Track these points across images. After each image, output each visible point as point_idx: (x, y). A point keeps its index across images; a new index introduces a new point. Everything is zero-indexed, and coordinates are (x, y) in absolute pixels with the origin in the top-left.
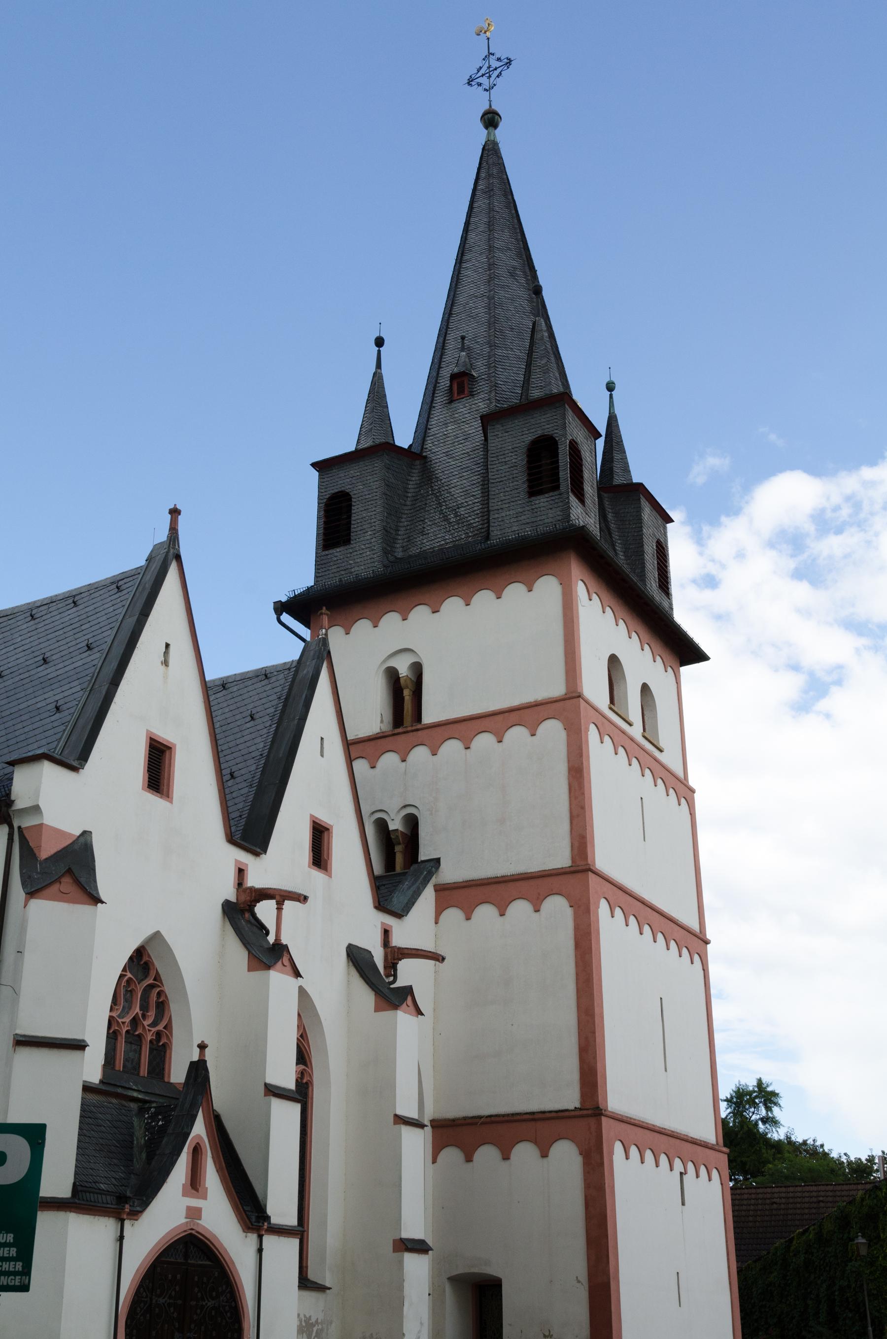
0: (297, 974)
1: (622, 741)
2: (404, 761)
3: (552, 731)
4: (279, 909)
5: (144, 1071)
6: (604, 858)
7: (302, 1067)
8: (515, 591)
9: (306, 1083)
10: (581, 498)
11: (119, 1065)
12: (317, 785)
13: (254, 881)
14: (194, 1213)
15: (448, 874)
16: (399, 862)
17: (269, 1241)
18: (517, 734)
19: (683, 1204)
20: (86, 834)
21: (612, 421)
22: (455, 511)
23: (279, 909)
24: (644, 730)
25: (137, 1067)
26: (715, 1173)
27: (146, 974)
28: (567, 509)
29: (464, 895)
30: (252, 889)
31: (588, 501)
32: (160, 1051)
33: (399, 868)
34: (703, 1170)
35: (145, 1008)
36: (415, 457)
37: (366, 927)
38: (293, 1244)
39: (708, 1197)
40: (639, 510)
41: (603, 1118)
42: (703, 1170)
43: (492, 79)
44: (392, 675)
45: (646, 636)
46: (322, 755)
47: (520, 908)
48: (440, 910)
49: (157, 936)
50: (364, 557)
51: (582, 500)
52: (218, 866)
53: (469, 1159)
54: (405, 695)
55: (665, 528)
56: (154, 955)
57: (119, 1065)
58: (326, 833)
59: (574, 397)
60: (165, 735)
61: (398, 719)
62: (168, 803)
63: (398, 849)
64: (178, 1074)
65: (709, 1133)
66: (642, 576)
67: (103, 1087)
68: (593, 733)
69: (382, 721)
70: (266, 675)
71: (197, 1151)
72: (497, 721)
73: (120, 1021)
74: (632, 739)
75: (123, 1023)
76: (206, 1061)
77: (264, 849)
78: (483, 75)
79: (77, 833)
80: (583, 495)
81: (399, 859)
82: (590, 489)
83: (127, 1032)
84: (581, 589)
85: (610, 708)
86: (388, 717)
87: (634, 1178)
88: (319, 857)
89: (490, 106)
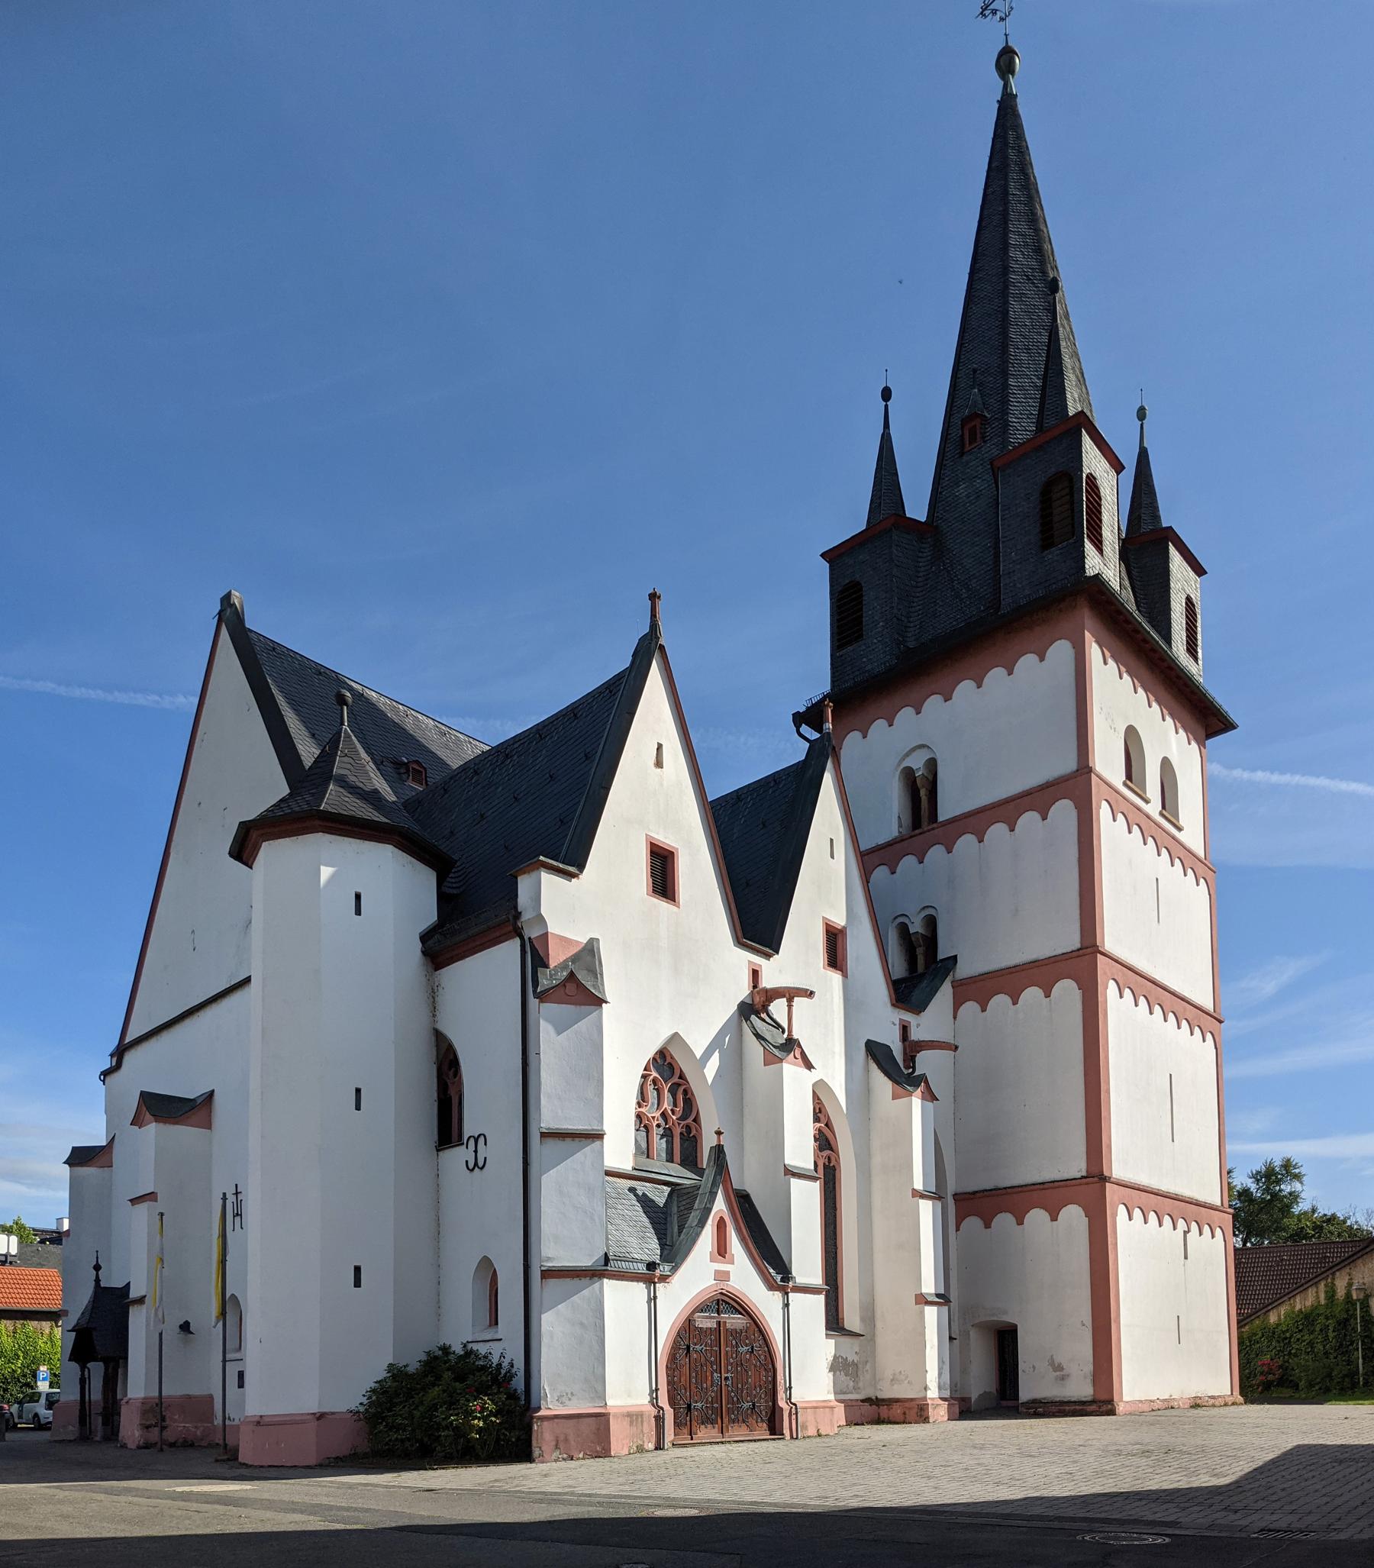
0: (809, 1066)
1: (1137, 821)
2: (921, 862)
4: (790, 1006)
6: (1113, 938)
7: (827, 1152)
12: (825, 881)
13: (767, 982)
14: (722, 1276)
15: (963, 970)
16: (919, 966)
17: (793, 1297)
18: (1029, 819)
19: (1186, 1258)
23: (790, 1006)
24: (1164, 807)
26: (1218, 1232)
28: (1081, 557)
29: (979, 989)
30: (766, 991)
33: (921, 968)
34: (1206, 1229)
38: (820, 1300)
39: (1213, 1251)
42: (1206, 1229)
44: (909, 775)
46: (832, 857)
48: (957, 1005)
49: (675, 1037)
51: (1100, 549)
54: (921, 791)
61: (916, 823)
63: (920, 951)
65: (1212, 1194)
66: (1168, 639)
69: (900, 826)
71: (721, 1225)
72: (1007, 810)
74: (1148, 817)
79: (583, 940)
80: (1101, 542)
84: (1094, 652)
86: (907, 820)
87: (1133, 1236)
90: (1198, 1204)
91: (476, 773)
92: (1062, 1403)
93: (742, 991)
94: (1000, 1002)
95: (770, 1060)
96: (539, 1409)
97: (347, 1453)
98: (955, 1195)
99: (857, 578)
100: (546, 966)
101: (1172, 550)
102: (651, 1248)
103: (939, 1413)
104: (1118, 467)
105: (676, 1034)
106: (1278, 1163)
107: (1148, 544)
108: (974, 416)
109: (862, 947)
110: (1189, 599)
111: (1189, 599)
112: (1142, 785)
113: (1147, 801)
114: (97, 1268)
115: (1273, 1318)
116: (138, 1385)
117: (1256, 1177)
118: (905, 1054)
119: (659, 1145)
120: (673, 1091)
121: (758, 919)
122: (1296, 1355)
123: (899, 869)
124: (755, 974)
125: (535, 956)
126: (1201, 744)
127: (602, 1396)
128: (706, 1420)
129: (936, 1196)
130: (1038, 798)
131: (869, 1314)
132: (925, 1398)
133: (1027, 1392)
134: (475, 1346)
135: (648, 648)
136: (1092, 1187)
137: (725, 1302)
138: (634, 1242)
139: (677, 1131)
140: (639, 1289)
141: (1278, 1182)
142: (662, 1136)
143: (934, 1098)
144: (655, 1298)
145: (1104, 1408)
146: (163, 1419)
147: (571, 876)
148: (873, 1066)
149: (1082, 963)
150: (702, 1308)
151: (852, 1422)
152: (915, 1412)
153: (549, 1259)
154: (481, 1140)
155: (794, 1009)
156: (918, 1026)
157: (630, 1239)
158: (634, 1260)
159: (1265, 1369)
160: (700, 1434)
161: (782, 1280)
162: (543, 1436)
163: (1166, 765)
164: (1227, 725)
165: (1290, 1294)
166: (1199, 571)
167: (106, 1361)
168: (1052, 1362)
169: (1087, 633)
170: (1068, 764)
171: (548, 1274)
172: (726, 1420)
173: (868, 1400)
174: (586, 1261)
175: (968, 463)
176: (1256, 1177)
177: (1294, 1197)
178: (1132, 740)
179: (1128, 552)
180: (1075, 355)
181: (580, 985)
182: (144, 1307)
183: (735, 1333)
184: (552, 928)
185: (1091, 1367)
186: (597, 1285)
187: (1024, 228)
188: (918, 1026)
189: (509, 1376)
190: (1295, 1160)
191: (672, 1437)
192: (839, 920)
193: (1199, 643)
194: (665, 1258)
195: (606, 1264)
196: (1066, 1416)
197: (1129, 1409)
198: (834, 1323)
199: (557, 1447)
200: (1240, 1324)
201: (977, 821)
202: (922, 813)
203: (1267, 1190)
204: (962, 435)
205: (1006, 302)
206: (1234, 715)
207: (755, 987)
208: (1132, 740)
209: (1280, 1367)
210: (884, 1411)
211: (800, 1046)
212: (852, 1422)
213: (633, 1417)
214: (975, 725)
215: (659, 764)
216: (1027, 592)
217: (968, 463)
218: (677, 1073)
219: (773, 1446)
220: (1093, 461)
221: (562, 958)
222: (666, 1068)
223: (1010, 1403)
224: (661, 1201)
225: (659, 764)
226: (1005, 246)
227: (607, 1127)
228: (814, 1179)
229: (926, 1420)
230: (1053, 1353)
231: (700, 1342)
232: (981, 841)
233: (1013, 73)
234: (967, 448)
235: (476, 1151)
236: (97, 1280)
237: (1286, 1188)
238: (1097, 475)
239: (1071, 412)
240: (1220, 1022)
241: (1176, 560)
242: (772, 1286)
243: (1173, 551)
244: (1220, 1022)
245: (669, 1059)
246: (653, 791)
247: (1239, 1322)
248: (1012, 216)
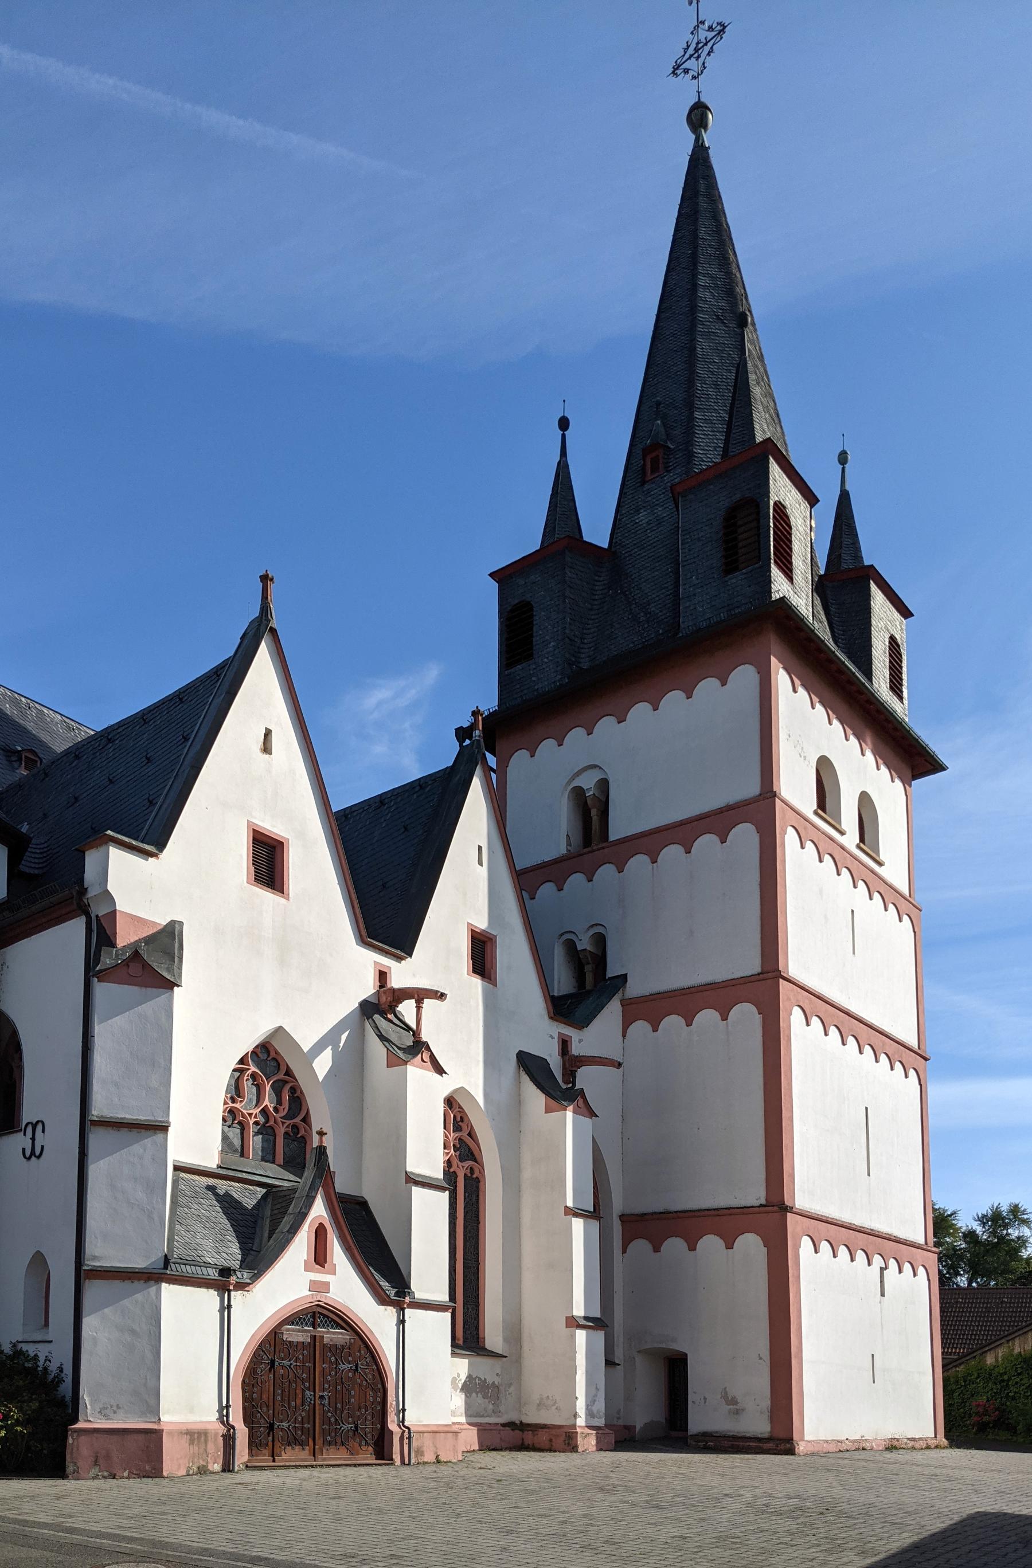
0: (440, 1070)
1: (828, 850)
2: (590, 880)
4: (419, 1008)
10: (788, 571)
12: (466, 888)
13: (396, 982)
15: (635, 988)
16: (583, 982)
18: (707, 842)
19: (883, 1295)
21: (844, 499)
23: (419, 1008)
26: (921, 1271)
28: (767, 582)
29: (651, 1009)
30: (394, 991)
33: (589, 985)
36: (607, 560)
40: (867, 596)
41: (789, 1214)
42: (907, 1267)
43: (695, 41)
44: (578, 793)
50: (546, 672)
51: (790, 578)
54: (591, 810)
58: (489, 944)
61: (587, 839)
62: (282, 901)
63: (588, 969)
65: (915, 1228)
66: (869, 674)
67: (221, 1171)
69: (569, 844)
70: (420, 786)
71: (320, 1233)
73: (245, 1112)
74: (843, 848)
75: (250, 1115)
76: (325, 1148)
77: (161, 844)
78: (689, 58)
79: (163, 922)
80: (791, 571)
81: (589, 978)
85: (858, 847)
86: (577, 839)
90: (897, 1241)
91: (77, 757)
92: (735, 1438)
93: (368, 988)
94: (673, 1022)
95: (393, 1061)
96: (76, 1420)
98: (622, 1217)
99: (524, 600)
100: (113, 945)
101: (873, 587)
102: (232, 1252)
103: (588, 1442)
104: (812, 499)
105: (280, 1029)
106: (1005, 1208)
107: (847, 581)
108: (655, 446)
109: (514, 954)
110: (892, 639)
111: (892, 639)
112: (838, 817)
113: (842, 833)
115: (990, 1360)
117: (983, 1220)
119: (255, 1142)
120: (277, 1090)
121: (389, 912)
122: (1013, 1398)
123: (566, 887)
124: (383, 976)
125: (101, 933)
126: (906, 782)
127: (154, 1409)
128: (293, 1441)
129: (595, 1214)
130: (719, 821)
131: (514, 1333)
132: (574, 1426)
133: (698, 1422)
134: (25, 1347)
135: (260, 628)
136: (771, 1217)
137: (320, 1315)
138: (208, 1244)
139: (281, 1131)
140: (210, 1298)
141: (1006, 1226)
142: (256, 1134)
143: (592, 1114)
144: (229, 1306)
145: (782, 1447)
147: (149, 854)
148: (525, 1079)
149: (763, 986)
150: (294, 1319)
151: (485, 1446)
152: (563, 1440)
153: (95, 1258)
154: (39, 1127)
155: (424, 1011)
156: (580, 1041)
157: (203, 1242)
158: (208, 1265)
159: (981, 1410)
160: (284, 1457)
161: (397, 1294)
162: (79, 1450)
163: (865, 801)
164: (934, 766)
165: (1009, 1336)
166: (905, 612)
168: (725, 1396)
169: (773, 658)
170: (752, 788)
172: (319, 1441)
173: (511, 1425)
174: (139, 1263)
175: (649, 491)
176: (983, 1220)
177: (1022, 1241)
179: (821, 586)
180: (769, 395)
181: (146, 966)
183: (333, 1349)
184: (122, 905)
185: (769, 1403)
186: (153, 1290)
187: (714, 271)
188: (580, 1041)
189: (58, 1380)
190: (1024, 1205)
191: (246, 1458)
192: (482, 924)
193: (905, 683)
194: (244, 1264)
195: (166, 1267)
196: (736, 1452)
197: (811, 1449)
198: (468, 1338)
199: (96, 1463)
200: (945, 1367)
201: (651, 842)
202: (593, 830)
203: (994, 1233)
204: (644, 465)
205: (693, 340)
207: (381, 987)
209: (997, 1409)
210: (529, 1438)
211: (428, 1048)
212: (485, 1446)
213: (195, 1436)
214: (649, 748)
215: (267, 749)
216: (708, 615)
217: (649, 491)
218: (283, 1070)
219: (376, 1474)
220: (781, 488)
221: (133, 939)
222: (269, 1063)
224: (249, 1202)
225: (267, 749)
226: (694, 287)
227: (172, 1119)
228: (441, 1189)
229: (574, 1449)
230: (726, 1383)
231: (288, 1356)
232: (654, 861)
233: (705, 127)
234: (649, 477)
235: (33, 1139)
237: (1014, 1233)
238: (787, 503)
239: (759, 438)
240: (926, 1059)
241: (878, 600)
242: (383, 1300)
243: (874, 588)
244: (926, 1059)
245: (273, 1054)
246: (256, 772)
247: (944, 1366)
248: (701, 259)
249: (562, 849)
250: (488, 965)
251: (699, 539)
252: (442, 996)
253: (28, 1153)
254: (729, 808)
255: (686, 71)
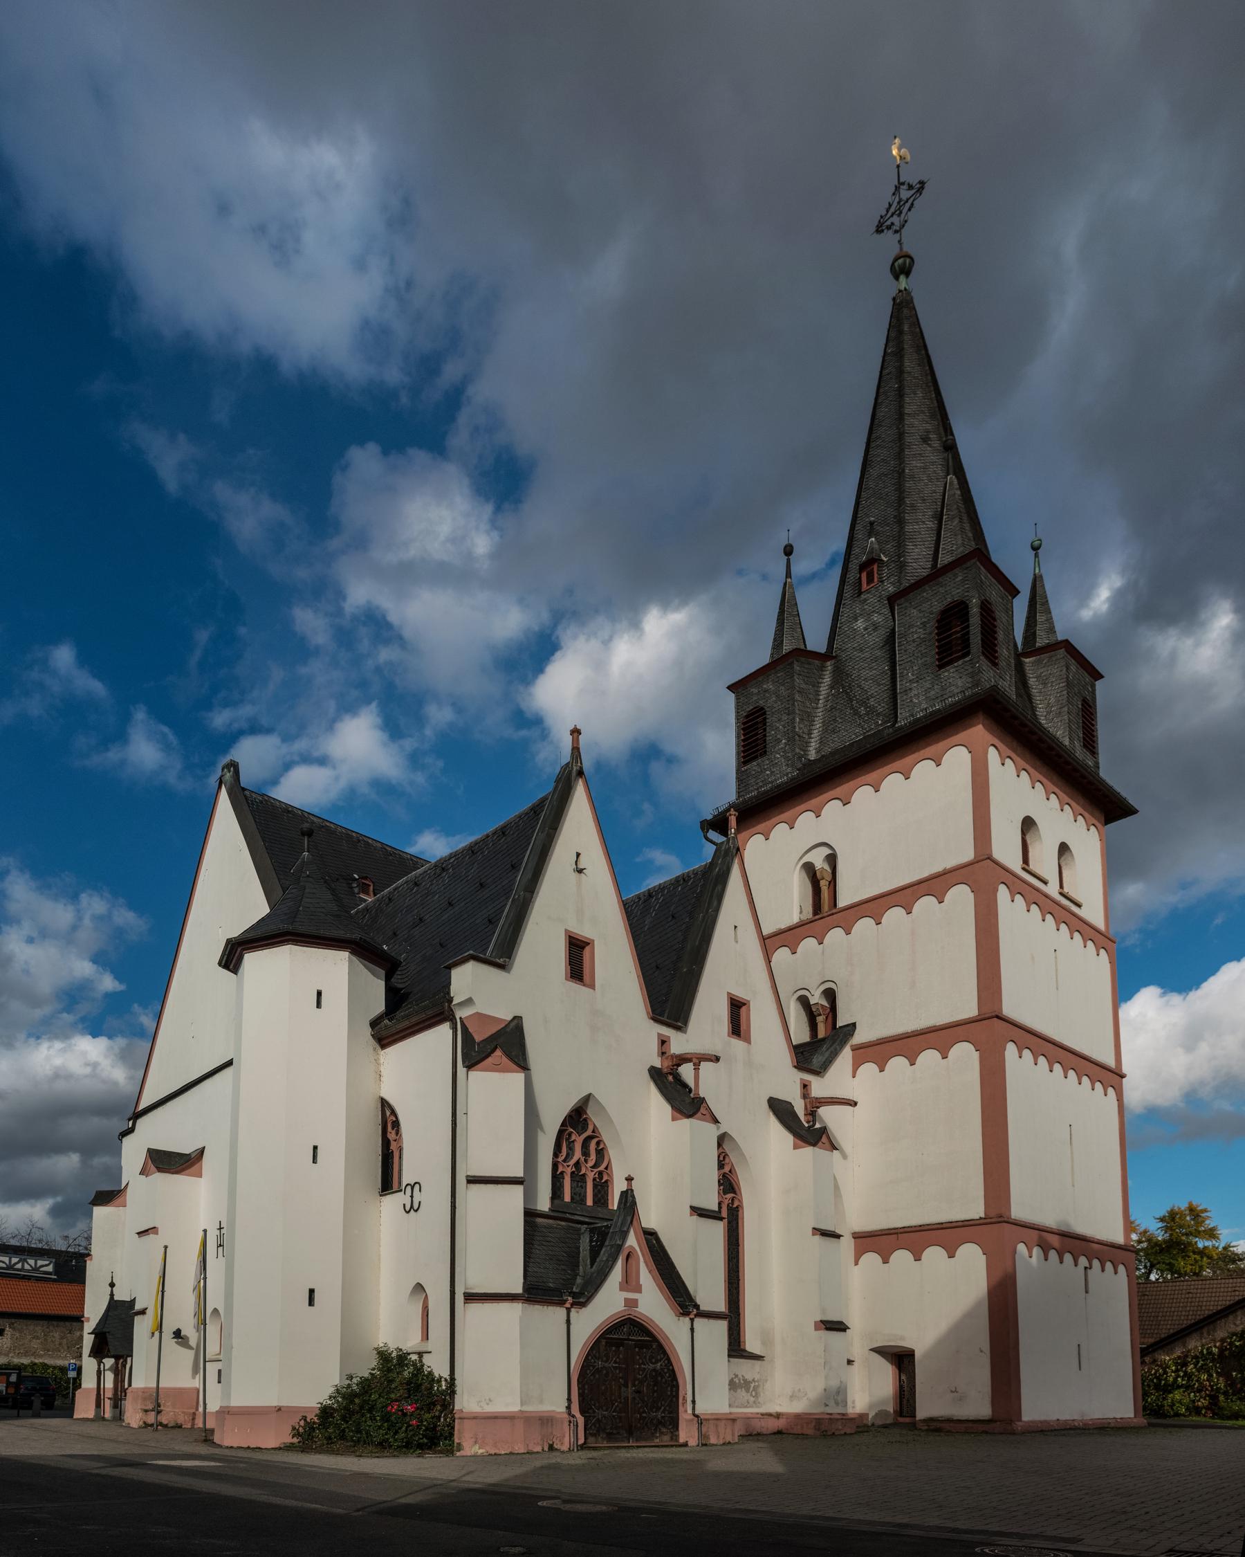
0: (716, 1121)
1: (1035, 897)
3: (961, 897)
4: (697, 1069)
5: (590, 1202)
7: (730, 1196)
8: (923, 769)
9: (606, 1181)
11: (567, 1198)
16: (823, 1037)
19: (1087, 1292)
20: (518, 1019)
21: (1037, 581)
22: (864, 703)
23: (697, 1069)
25: (583, 1200)
27: (585, 1128)
29: (880, 1051)
31: (1002, 664)
32: (602, 1188)
33: (822, 1032)
35: (586, 1153)
37: (787, 1083)
38: (723, 1325)
44: (809, 868)
45: (1079, 809)
47: (929, 1057)
50: (778, 769)
52: (642, 1038)
53: (886, 1261)
55: (1093, 686)
56: (590, 1112)
57: (567, 1198)
59: (994, 560)
60: (584, 931)
61: (817, 907)
63: (820, 1019)
64: (614, 1203)
68: (1003, 893)
72: (904, 896)
74: (1046, 896)
79: (509, 1018)
82: (1004, 652)
83: (572, 1173)
88: (737, 1027)
89: (901, 249)
91: (416, 884)
97: (764, 658)
113: (1045, 883)
114: (112, 1285)
116: (141, 1378)
118: (806, 1108)
123: (799, 950)
124: (663, 1042)
146: (159, 1406)
167: (117, 1358)
171: (470, 1297)
175: (865, 600)
178: (1028, 824)
182: (146, 1317)
198: (736, 1349)
201: (874, 907)
206: (1133, 801)
207: (663, 1053)
208: (1028, 824)
216: (924, 706)
217: (865, 600)
223: (908, 1420)
236: (112, 1295)
246: (580, 888)
249: (795, 919)
250: (743, 1027)
251: (914, 641)
252: (717, 1059)
253: (408, 1208)
254: (945, 873)
255: (889, 228)
